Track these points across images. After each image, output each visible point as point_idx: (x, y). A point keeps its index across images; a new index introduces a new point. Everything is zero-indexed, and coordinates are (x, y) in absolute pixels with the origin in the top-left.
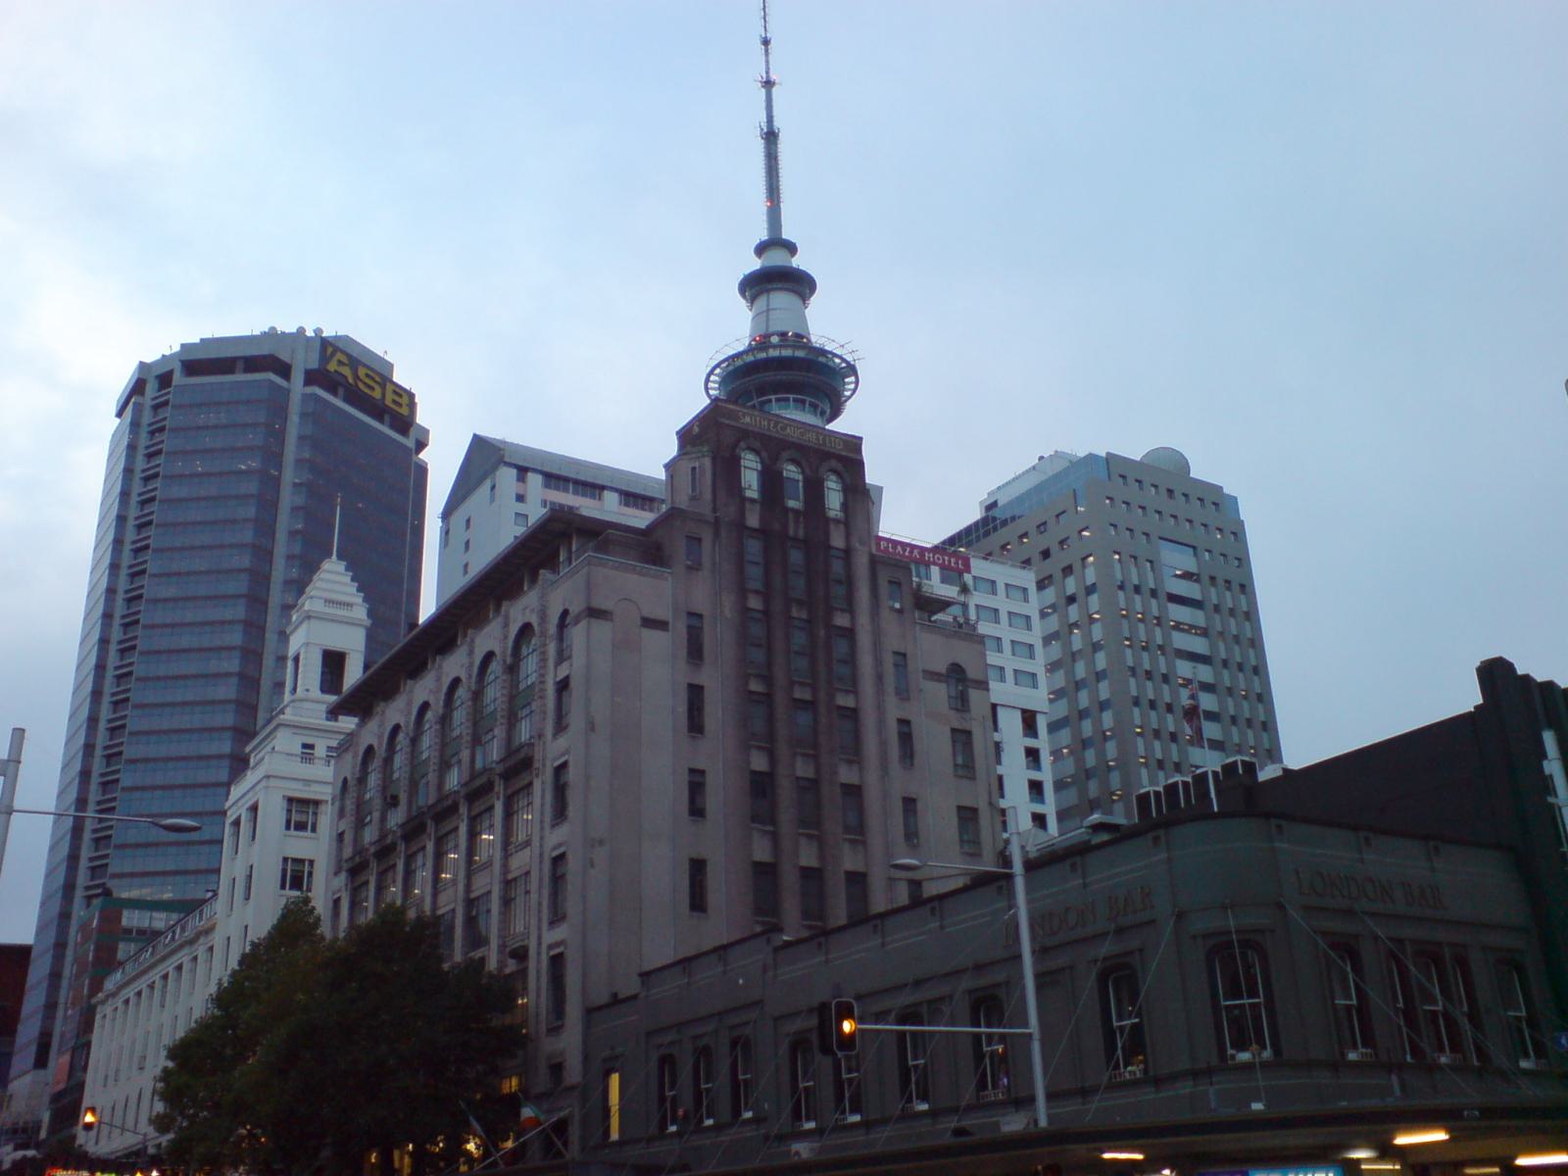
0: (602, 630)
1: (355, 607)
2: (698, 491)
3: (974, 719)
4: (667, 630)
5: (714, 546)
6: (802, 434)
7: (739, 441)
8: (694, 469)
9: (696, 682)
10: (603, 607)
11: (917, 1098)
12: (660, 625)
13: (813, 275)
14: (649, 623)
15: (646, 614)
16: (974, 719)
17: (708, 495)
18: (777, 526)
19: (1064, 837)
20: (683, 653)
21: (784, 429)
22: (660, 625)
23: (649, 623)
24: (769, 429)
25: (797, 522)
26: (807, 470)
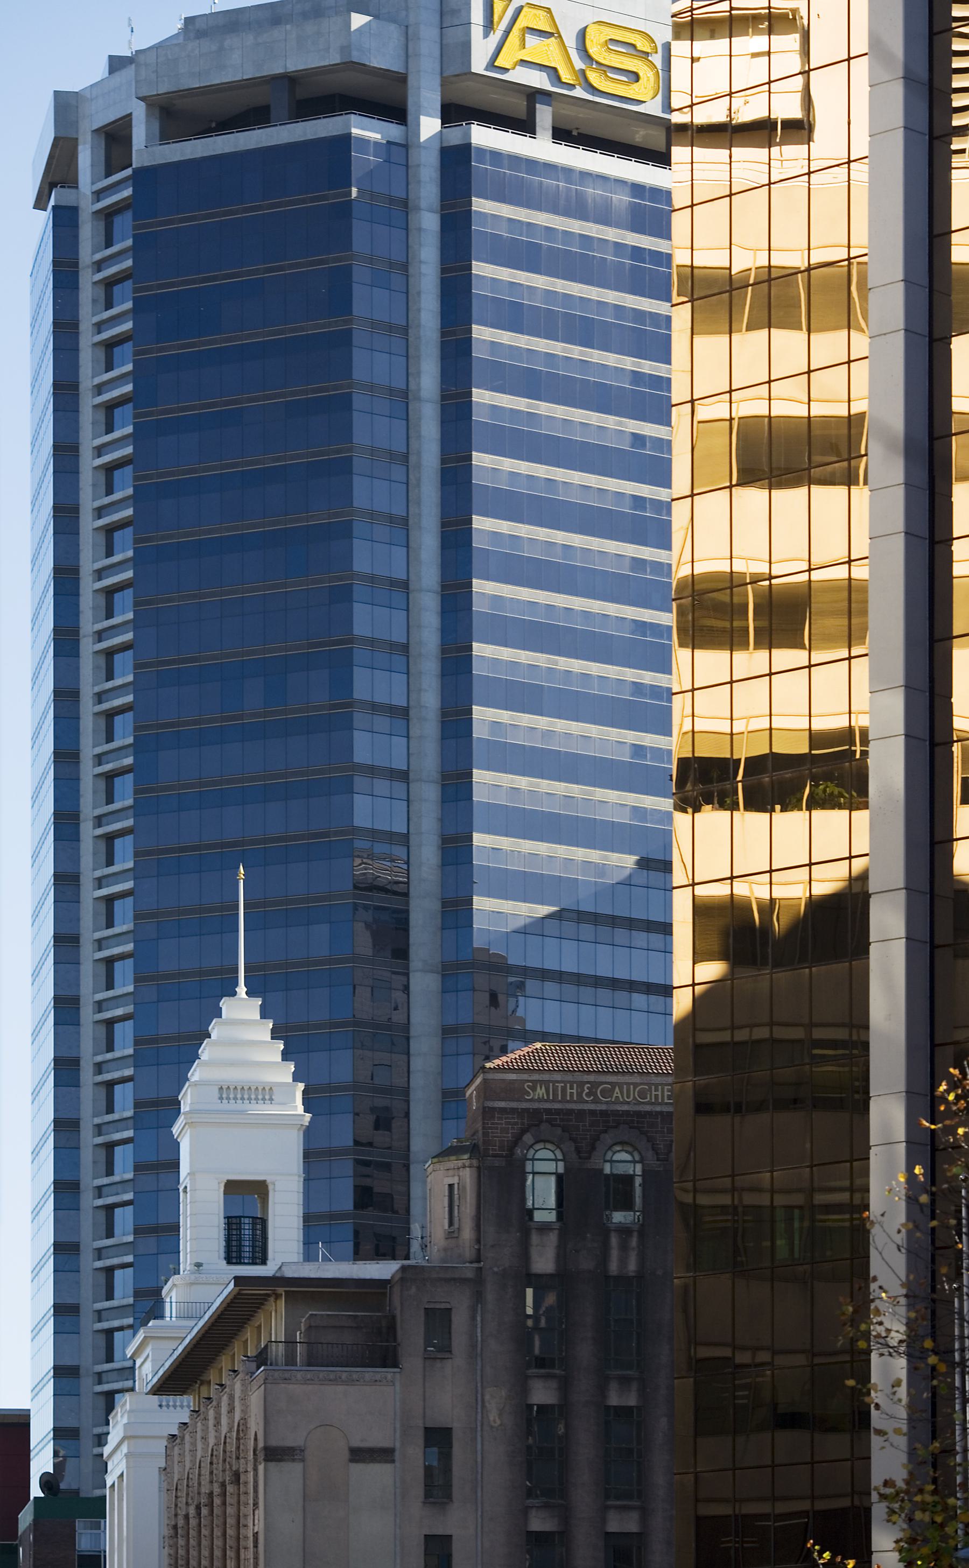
0: (291, 1472)
1: (406, 1120)
2: (456, 1226)
3: (425, 263)
4: (393, 1461)
5: (473, 1318)
6: (642, 1094)
7: (524, 1131)
8: (451, 1186)
9: (440, 1531)
10: (289, 1443)
11: (671, 627)
12: (383, 1455)
13: (575, 34)
14: (359, 1455)
15: (356, 1443)
16: (425, 263)
17: (467, 1234)
18: (586, 1263)
19: (731, 957)
20: (418, 1490)
21: (607, 1093)
22: (383, 1455)
23: (359, 1455)
24: (581, 1100)
25: (624, 1247)
26: (650, 1155)
